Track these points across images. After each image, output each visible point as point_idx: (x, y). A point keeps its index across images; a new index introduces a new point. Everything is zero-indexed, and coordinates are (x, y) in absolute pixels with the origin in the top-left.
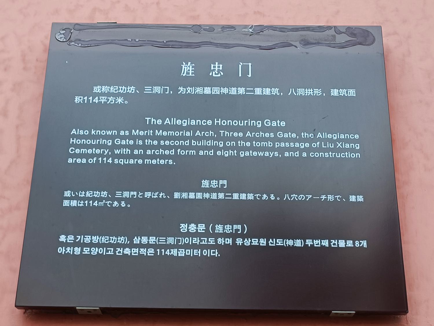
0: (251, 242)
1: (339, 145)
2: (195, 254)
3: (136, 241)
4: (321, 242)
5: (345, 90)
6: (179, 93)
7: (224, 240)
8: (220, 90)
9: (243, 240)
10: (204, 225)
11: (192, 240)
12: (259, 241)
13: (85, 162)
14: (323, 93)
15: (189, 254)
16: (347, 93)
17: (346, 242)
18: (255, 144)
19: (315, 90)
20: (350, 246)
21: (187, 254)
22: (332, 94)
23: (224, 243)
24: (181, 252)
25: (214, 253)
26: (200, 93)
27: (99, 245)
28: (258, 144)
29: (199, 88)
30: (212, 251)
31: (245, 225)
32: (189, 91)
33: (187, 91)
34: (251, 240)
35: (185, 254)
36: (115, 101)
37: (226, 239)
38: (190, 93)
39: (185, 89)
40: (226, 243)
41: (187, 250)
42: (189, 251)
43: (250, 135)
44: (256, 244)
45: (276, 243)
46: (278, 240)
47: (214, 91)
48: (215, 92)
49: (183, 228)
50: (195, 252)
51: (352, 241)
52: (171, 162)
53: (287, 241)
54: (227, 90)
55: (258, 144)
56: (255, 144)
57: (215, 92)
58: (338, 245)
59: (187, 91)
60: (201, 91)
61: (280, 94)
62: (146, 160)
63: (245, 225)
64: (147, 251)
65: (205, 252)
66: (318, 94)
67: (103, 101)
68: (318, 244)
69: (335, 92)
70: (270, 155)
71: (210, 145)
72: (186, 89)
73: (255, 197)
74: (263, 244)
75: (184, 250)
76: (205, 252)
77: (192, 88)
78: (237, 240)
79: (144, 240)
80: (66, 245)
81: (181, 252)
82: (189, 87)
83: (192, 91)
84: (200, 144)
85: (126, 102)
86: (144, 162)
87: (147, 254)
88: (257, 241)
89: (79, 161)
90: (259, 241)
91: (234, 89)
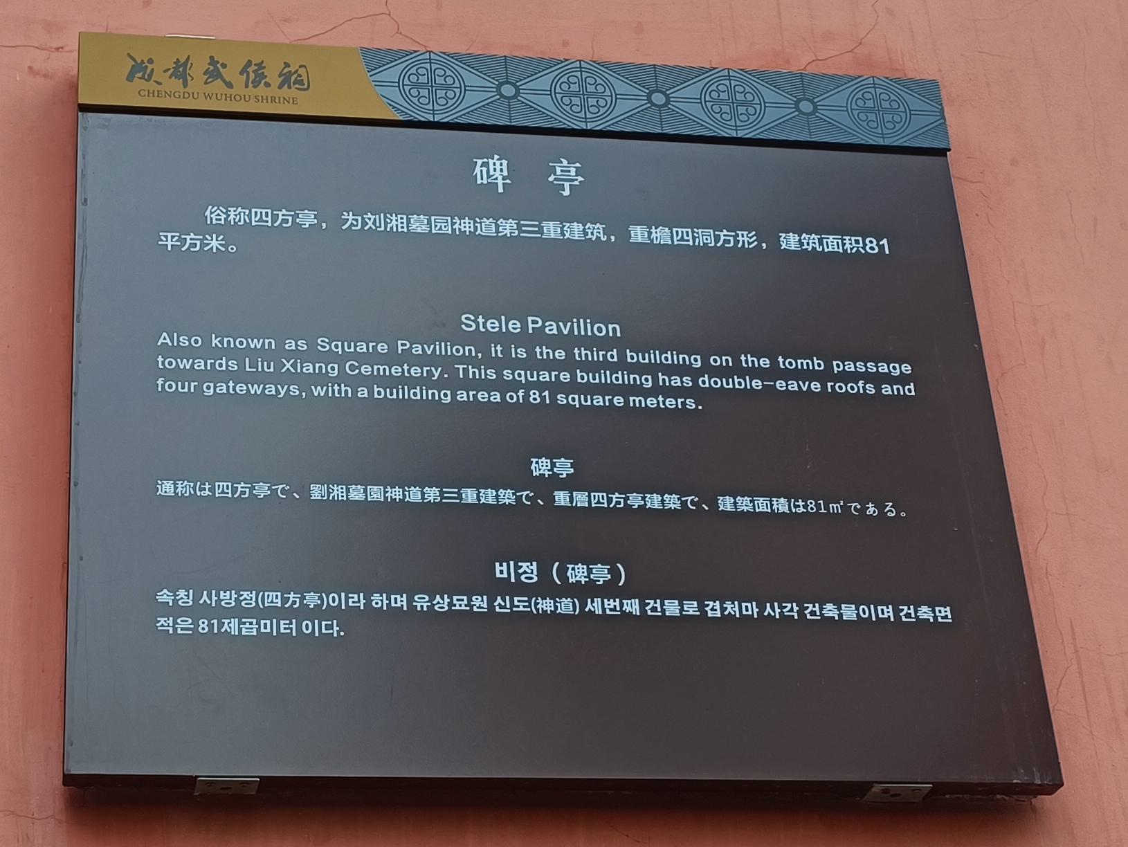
0: (451, 604)
1: (288, 366)
2: (282, 631)
4: (622, 605)
5: (816, 237)
7: (389, 599)
9: (432, 599)
11: (347, 599)
12: (470, 600)
13: (499, 400)
14: (760, 241)
15: (268, 630)
16: (821, 243)
17: (681, 605)
18: (163, 363)
19: (740, 233)
20: (691, 613)
21: (263, 630)
22: (784, 246)
23: (389, 605)
24: (248, 625)
25: (329, 627)
27: (260, 613)
28: (170, 363)
30: (324, 623)
32: (370, 224)
33: (364, 223)
34: (450, 597)
35: (258, 630)
36: (203, 245)
37: (393, 597)
39: (360, 218)
40: (393, 604)
41: (262, 622)
42: (268, 622)
43: (168, 341)
44: (463, 608)
45: (512, 605)
46: (516, 599)
49: (525, 572)
50: (282, 626)
51: (695, 603)
52: (691, 404)
53: (540, 600)
55: (170, 363)
56: (163, 363)
57: (440, 229)
58: (663, 611)
59: (364, 223)
61: (609, 238)
62: (631, 399)
64: (175, 622)
65: (307, 627)
66: (749, 243)
67: (169, 243)
68: (614, 609)
69: (790, 241)
70: (278, 392)
71: (670, 362)
72: (363, 219)
73: (519, 499)
74: (479, 607)
75: (254, 621)
76: (307, 627)
78: (416, 598)
80: (175, 611)
81: (248, 625)
84: (647, 361)
85: (232, 249)
86: (627, 401)
87: (175, 629)
88: (466, 602)
89: (482, 396)
90: (470, 600)
91: (488, 222)
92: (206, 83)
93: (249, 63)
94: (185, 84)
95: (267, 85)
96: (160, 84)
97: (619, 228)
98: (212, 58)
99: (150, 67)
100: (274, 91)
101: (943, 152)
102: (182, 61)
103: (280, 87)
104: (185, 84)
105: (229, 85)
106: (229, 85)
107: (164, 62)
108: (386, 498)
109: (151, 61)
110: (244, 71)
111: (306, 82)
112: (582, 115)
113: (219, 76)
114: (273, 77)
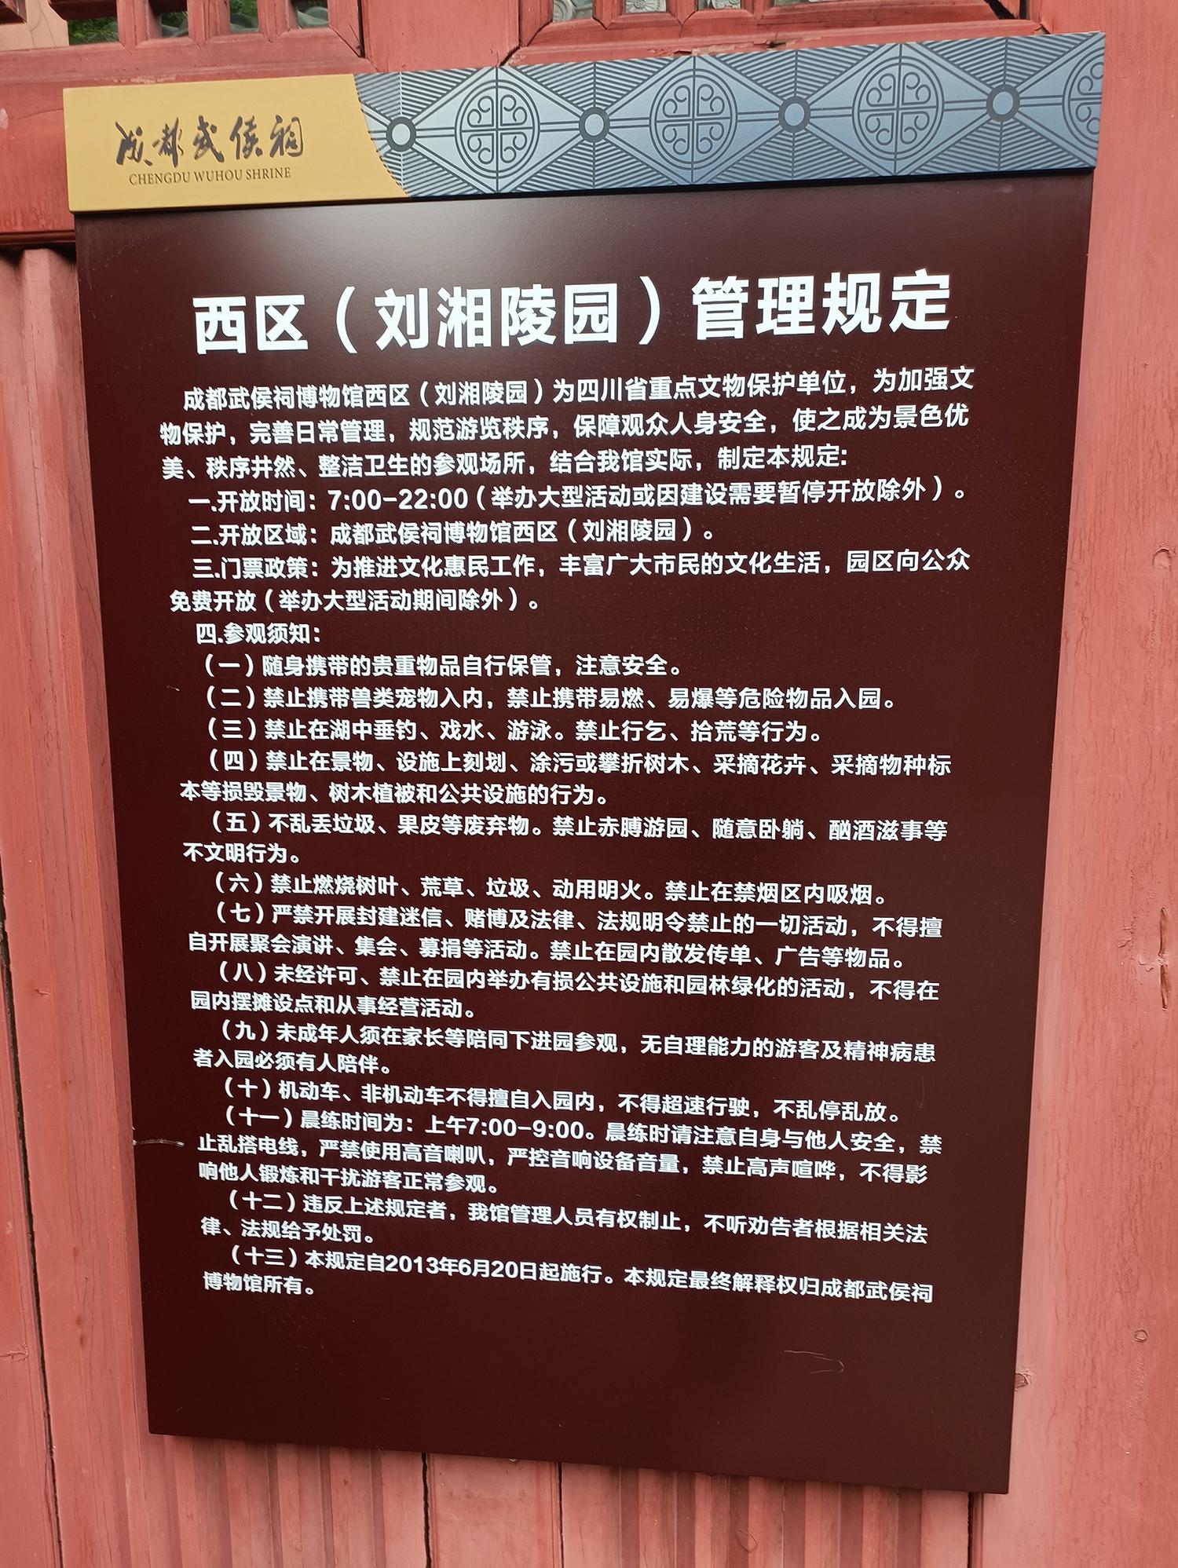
3: (586, 665)
6: (876, 390)
8: (709, 983)
10: (803, 964)
26: (472, 342)
29: (464, 294)
31: (646, 280)
38: (402, 341)
47: (576, 319)
48: (588, 329)
54: (789, 300)
57: (588, 329)
60: (479, 324)
63: (646, 280)
77: (411, 298)
79: (610, 664)
82: (390, 292)
83: (411, 331)
92: (196, 157)
93: (240, 119)
94: (175, 163)
95: (259, 152)
96: (149, 164)
97: (834, 557)
98: (201, 118)
99: (139, 139)
100: (265, 161)
101: (1087, 172)
102: (171, 128)
103: (272, 155)
104: (175, 163)
105: (220, 157)
106: (220, 157)
107: (151, 136)
108: (867, 1056)
109: (279, 119)
110: (234, 135)
111: (298, 143)
112: (891, 148)
113: (210, 145)
114: (265, 143)
